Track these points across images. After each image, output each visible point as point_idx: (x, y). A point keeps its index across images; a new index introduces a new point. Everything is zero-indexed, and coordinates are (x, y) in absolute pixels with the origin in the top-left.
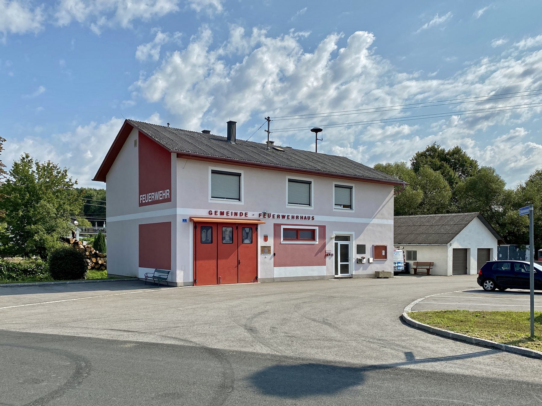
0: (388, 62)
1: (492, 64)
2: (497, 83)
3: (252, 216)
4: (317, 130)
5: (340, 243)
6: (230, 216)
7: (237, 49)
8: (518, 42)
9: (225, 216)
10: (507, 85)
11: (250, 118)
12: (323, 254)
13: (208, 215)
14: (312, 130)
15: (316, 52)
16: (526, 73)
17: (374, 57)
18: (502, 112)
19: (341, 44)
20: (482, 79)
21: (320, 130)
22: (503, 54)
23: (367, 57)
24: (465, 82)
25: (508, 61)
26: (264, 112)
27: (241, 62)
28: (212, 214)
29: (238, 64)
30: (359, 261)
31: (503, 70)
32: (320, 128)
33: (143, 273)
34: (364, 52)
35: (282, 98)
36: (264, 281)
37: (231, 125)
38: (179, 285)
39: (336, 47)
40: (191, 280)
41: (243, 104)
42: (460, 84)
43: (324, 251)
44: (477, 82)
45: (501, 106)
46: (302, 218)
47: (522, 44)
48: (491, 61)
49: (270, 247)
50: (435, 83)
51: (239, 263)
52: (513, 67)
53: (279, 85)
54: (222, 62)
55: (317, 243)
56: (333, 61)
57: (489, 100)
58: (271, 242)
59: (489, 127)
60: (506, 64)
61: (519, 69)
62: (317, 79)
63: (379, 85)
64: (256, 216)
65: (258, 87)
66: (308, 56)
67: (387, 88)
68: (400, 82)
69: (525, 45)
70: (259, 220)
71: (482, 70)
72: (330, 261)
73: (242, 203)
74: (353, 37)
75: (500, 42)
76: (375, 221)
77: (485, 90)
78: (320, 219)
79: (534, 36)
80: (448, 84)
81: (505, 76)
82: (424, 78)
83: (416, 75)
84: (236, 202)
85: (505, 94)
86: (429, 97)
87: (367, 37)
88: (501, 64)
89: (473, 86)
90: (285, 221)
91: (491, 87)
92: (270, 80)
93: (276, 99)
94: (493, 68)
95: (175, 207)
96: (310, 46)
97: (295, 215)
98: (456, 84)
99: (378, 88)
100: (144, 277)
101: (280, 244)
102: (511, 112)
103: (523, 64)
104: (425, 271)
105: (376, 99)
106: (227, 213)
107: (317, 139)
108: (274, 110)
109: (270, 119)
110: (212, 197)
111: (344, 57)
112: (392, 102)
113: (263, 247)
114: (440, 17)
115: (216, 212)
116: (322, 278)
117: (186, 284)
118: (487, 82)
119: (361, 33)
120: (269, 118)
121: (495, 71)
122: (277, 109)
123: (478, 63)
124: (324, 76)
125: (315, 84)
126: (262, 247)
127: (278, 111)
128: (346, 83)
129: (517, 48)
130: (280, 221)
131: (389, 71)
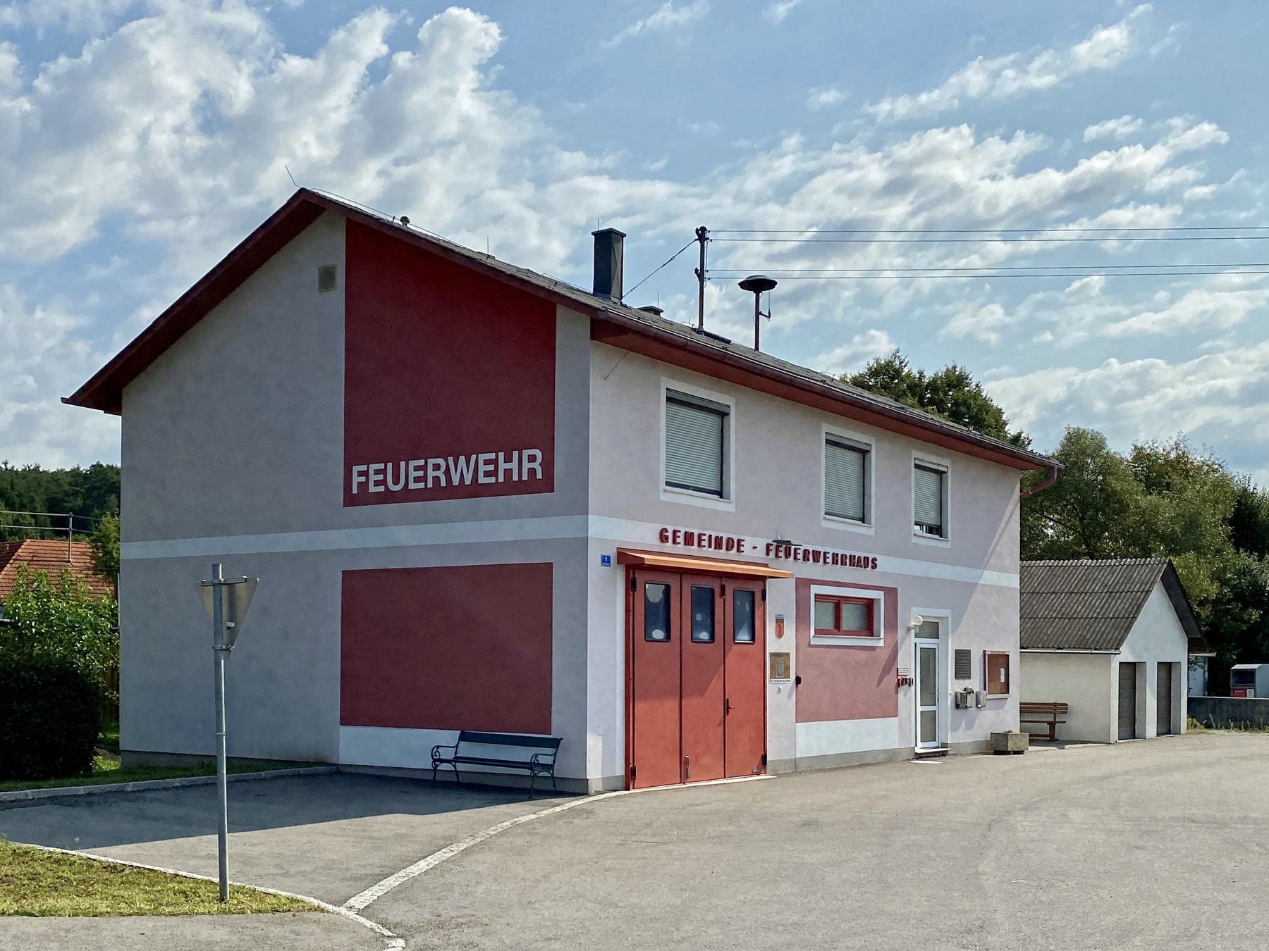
0: (537, 112)
1: (810, 154)
2: (821, 207)
3: (752, 555)
7: (65, 17)
8: (875, 102)
10: (846, 216)
11: (95, 234)
13: (656, 541)
14: (743, 285)
15: (323, 56)
16: (896, 188)
17: (493, 94)
18: (835, 283)
19: (399, 39)
20: (784, 192)
21: (770, 284)
22: (837, 129)
23: (474, 91)
24: (739, 197)
25: (850, 151)
26: (144, 219)
27: (77, 54)
29: (63, 60)
31: (840, 172)
32: (770, 276)
33: (364, 746)
34: (468, 80)
35: (208, 183)
37: (607, 244)
38: (593, 787)
39: (385, 49)
40: (620, 770)
41: (73, 190)
42: (728, 200)
44: (769, 200)
45: (832, 267)
47: (885, 107)
48: (806, 147)
50: (661, 189)
51: (727, 708)
52: (861, 167)
53: (196, 142)
54: (15, 47)
55: (881, 644)
56: (371, 88)
57: (805, 250)
59: (802, 324)
60: (845, 158)
61: (875, 173)
62: (322, 139)
63: (509, 178)
65: (127, 143)
66: (295, 65)
67: (528, 190)
68: (562, 178)
69: (891, 113)
70: (766, 565)
71: (785, 166)
72: (910, 701)
74: (439, 26)
75: (829, 97)
77: (795, 221)
79: (914, 93)
80: (694, 195)
81: (841, 190)
82: (630, 171)
83: (609, 161)
84: (713, 503)
85: (839, 237)
86: (644, 227)
87: (478, 32)
88: (833, 156)
89: (760, 210)
91: (806, 216)
92: (170, 119)
93: (185, 183)
94: (812, 165)
95: (581, 508)
96: (304, 34)
98: (715, 199)
99: (504, 186)
100: (427, 764)
102: (858, 285)
103: (886, 163)
104: (1045, 728)
105: (497, 219)
107: (758, 313)
108: (180, 217)
109: (708, 235)
110: (668, 484)
111: (406, 82)
112: (544, 231)
114: (676, 8)
116: (889, 758)
118: (795, 200)
119: (467, 15)
120: (703, 229)
121: (812, 175)
122: (188, 215)
123: (772, 146)
124: (346, 133)
125: (315, 151)
127: (192, 222)
128: (409, 160)
129: (871, 120)
131: (536, 143)
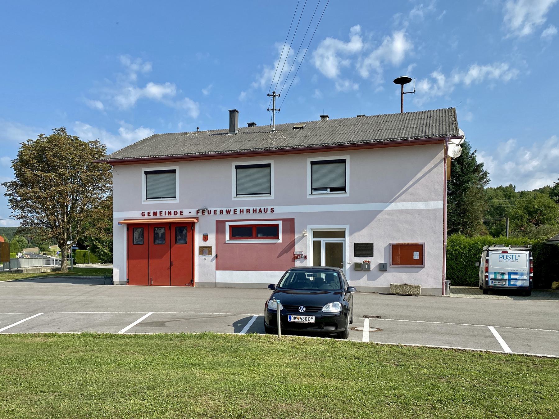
3: (188, 213)
4: (402, 81)
5: (324, 241)
6: (163, 216)
9: (158, 216)
12: (289, 255)
21: (408, 80)
28: (144, 215)
30: (358, 267)
36: (203, 285)
43: (292, 251)
46: (255, 211)
49: (211, 247)
58: (212, 242)
64: (193, 213)
73: (177, 201)
76: (393, 206)
78: (284, 211)
90: (231, 216)
97: (251, 208)
101: (225, 243)
106: (161, 213)
113: (202, 249)
115: (149, 213)
117: (121, 283)
126: (200, 247)
130: (224, 217)
